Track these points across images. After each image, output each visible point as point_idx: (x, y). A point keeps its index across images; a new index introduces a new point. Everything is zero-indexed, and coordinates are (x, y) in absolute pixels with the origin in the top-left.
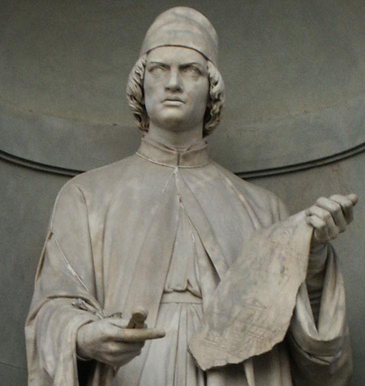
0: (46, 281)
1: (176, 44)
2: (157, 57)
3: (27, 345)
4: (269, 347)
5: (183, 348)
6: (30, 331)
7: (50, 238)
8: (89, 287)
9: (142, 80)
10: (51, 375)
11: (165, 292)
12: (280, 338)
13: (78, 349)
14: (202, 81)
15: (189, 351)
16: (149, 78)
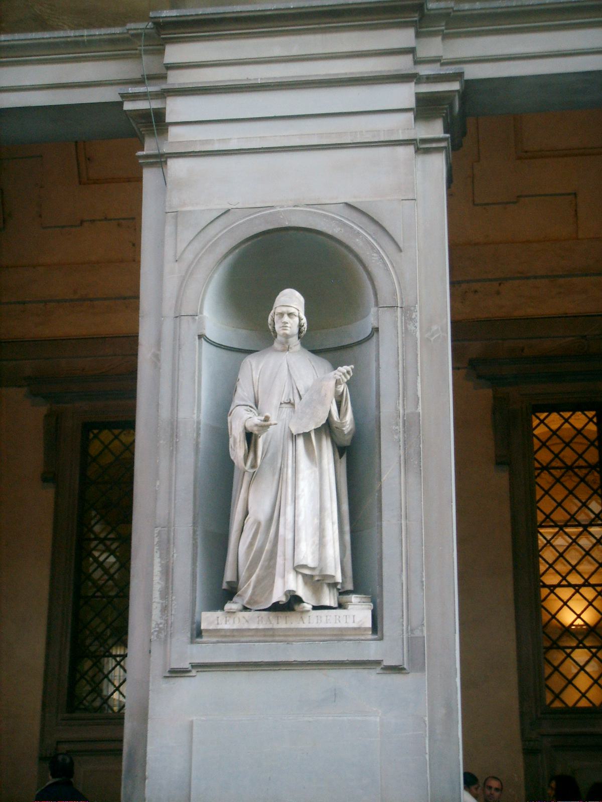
0: (237, 401)
1: (335, 202)
2: (279, 310)
3: (154, 592)
4: (320, 425)
5: (287, 427)
6: (229, 419)
7: (230, 415)
8: (253, 401)
9: (274, 319)
10: (581, 469)
11: (281, 404)
12: (324, 422)
13: (245, 428)
14: (297, 319)
15: (289, 427)
16: (276, 318)
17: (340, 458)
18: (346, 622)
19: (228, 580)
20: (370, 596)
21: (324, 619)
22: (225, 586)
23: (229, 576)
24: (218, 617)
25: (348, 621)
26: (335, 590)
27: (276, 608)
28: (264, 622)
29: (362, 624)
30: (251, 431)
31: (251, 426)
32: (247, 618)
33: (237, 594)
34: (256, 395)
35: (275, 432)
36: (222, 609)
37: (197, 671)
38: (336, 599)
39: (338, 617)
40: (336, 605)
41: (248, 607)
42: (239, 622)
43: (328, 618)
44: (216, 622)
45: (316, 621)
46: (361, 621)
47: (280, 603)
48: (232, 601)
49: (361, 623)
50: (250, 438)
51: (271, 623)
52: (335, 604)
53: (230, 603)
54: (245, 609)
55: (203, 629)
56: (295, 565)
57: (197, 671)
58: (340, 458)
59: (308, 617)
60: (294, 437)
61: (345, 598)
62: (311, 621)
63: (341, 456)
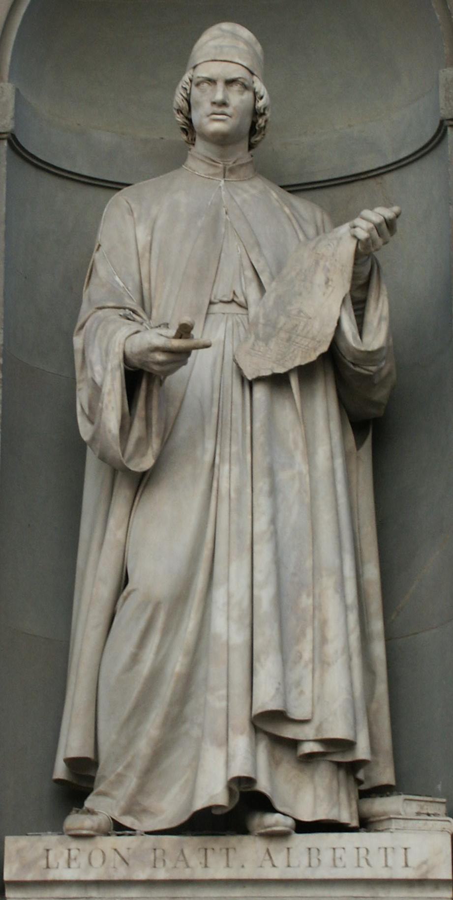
0: (93, 293)
2: (203, 72)
4: (313, 357)
5: (229, 358)
8: (136, 297)
9: (189, 95)
12: (324, 348)
13: (126, 359)
15: (234, 360)
16: (196, 92)
17: (358, 449)
18: (386, 866)
19: (74, 753)
20: (444, 800)
21: (327, 856)
22: (60, 771)
23: (73, 743)
24: (48, 850)
25: (390, 863)
26: (352, 779)
27: (204, 824)
28: (169, 864)
29: (427, 872)
30: (139, 366)
31: (140, 353)
32: (124, 852)
33: (95, 792)
34: (146, 285)
35: (201, 373)
36: (57, 828)
37: (406, 800)
38: (354, 806)
39: (363, 852)
40: (355, 823)
41: (127, 821)
42: (104, 862)
43: (339, 853)
44: (43, 863)
45: (305, 861)
46: (425, 862)
47: (214, 812)
48: (81, 811)
49: (425, 868)
50: (137, 378)
51: (188, 867)
52: (351, 818)
53: (77, 812)
54: (119, 828)
55: (242, 734)
56: (258, 709)
57: (406, 800)
58: (358, 449)
59: (286, 851)
60: (249, 384)
61: (379, 805)
62: (294, 862)
63: (359, 444)
